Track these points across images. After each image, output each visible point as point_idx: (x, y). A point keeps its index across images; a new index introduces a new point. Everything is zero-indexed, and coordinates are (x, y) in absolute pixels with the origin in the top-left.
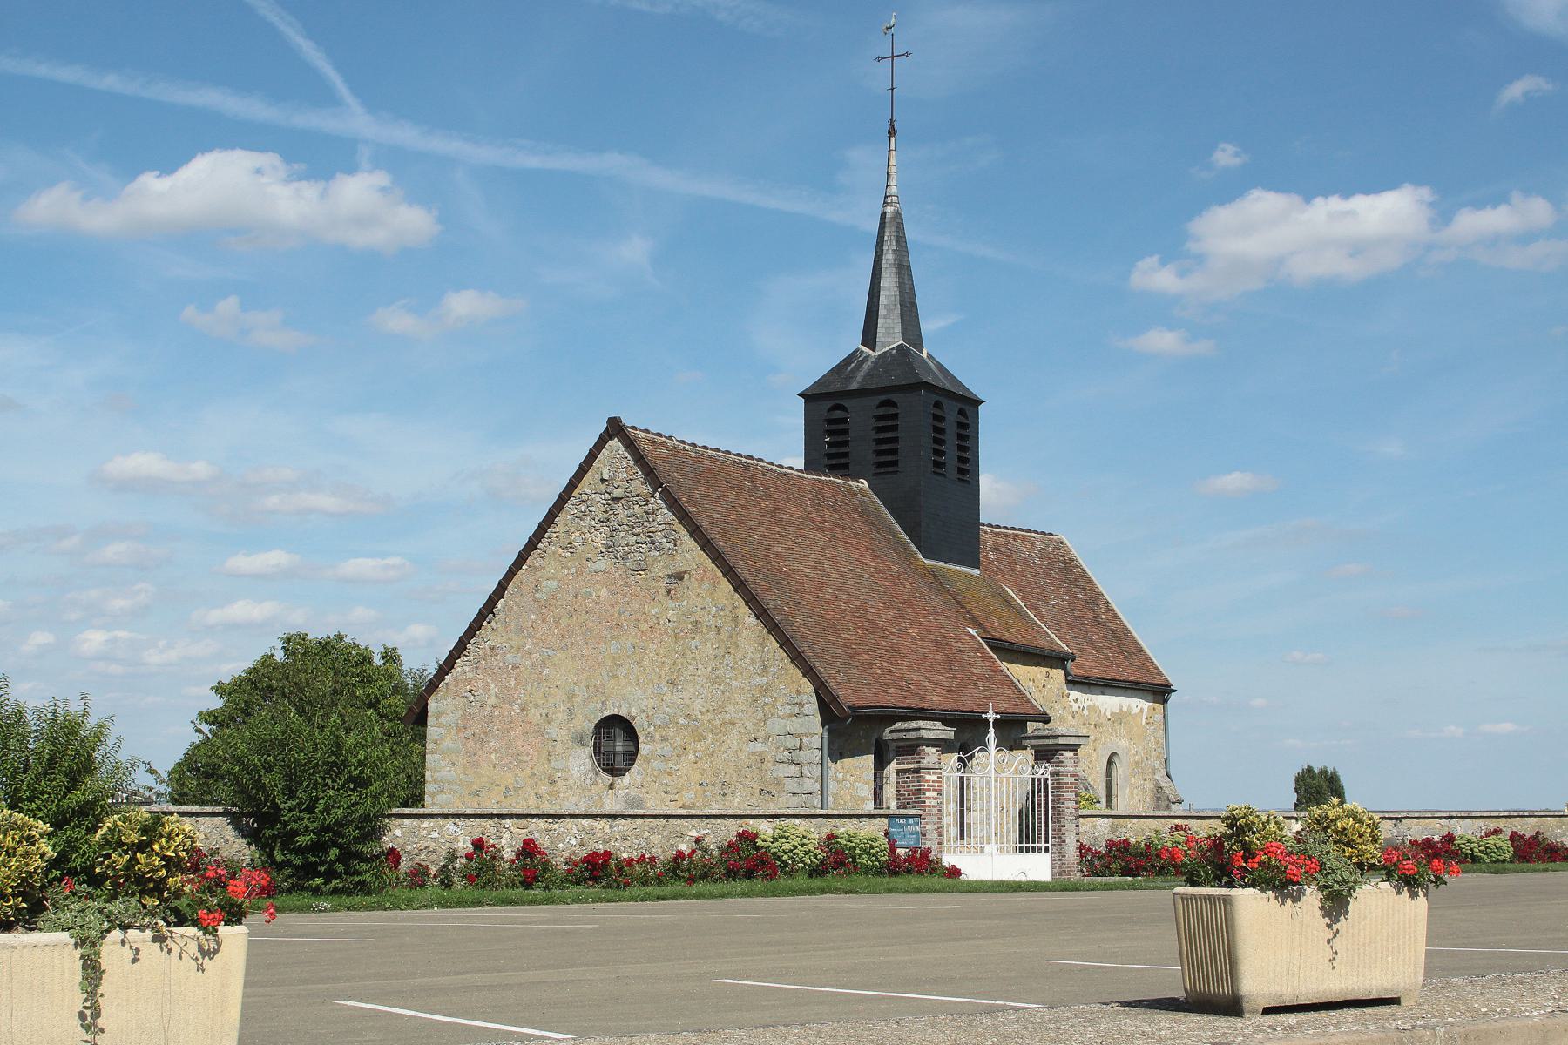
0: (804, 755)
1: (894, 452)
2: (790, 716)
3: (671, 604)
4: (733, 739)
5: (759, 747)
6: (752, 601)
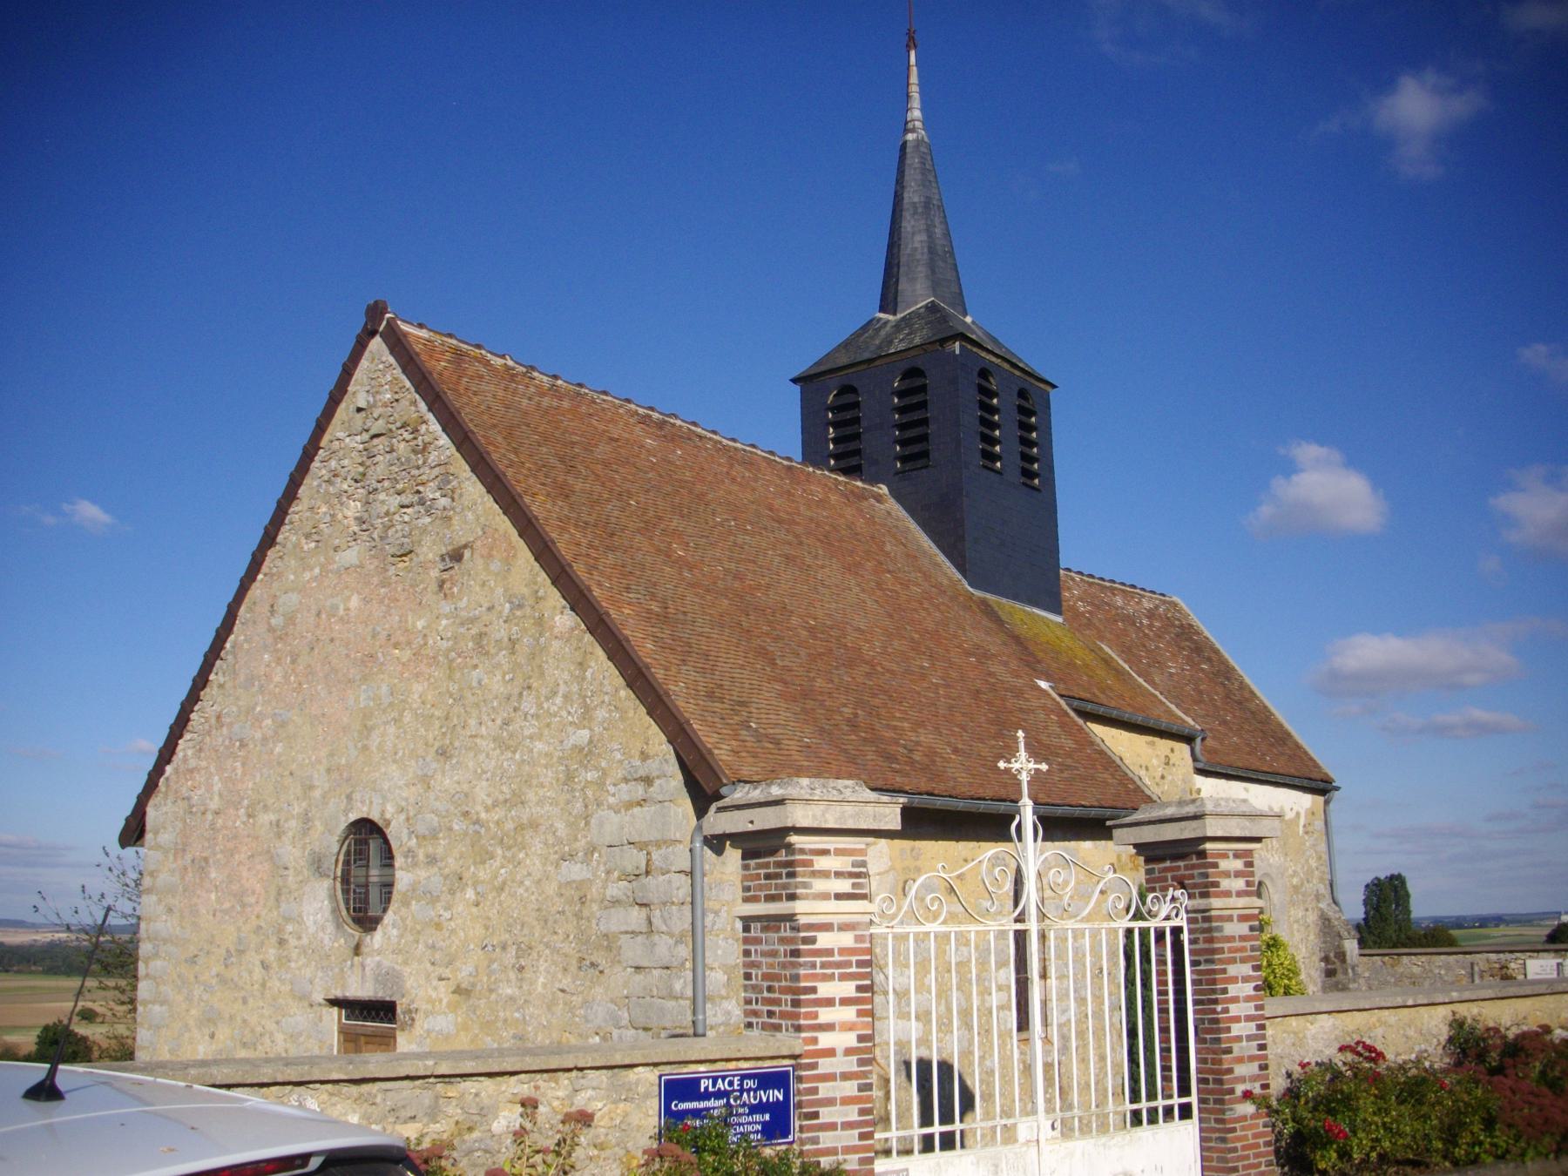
0: (654, 886)
1: (924, 438)
2: (630, 805)
3: (446, 608)
4: (534, 860)
5: (576, 871)
6: (561, 576)
